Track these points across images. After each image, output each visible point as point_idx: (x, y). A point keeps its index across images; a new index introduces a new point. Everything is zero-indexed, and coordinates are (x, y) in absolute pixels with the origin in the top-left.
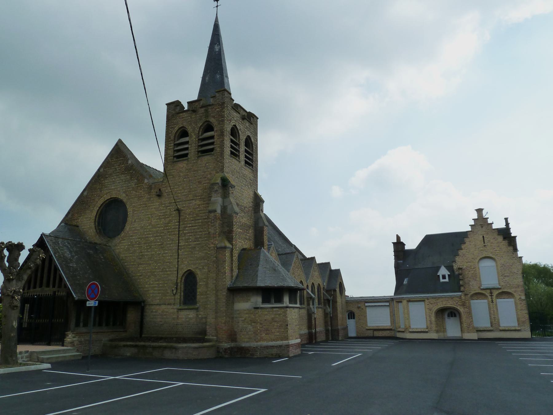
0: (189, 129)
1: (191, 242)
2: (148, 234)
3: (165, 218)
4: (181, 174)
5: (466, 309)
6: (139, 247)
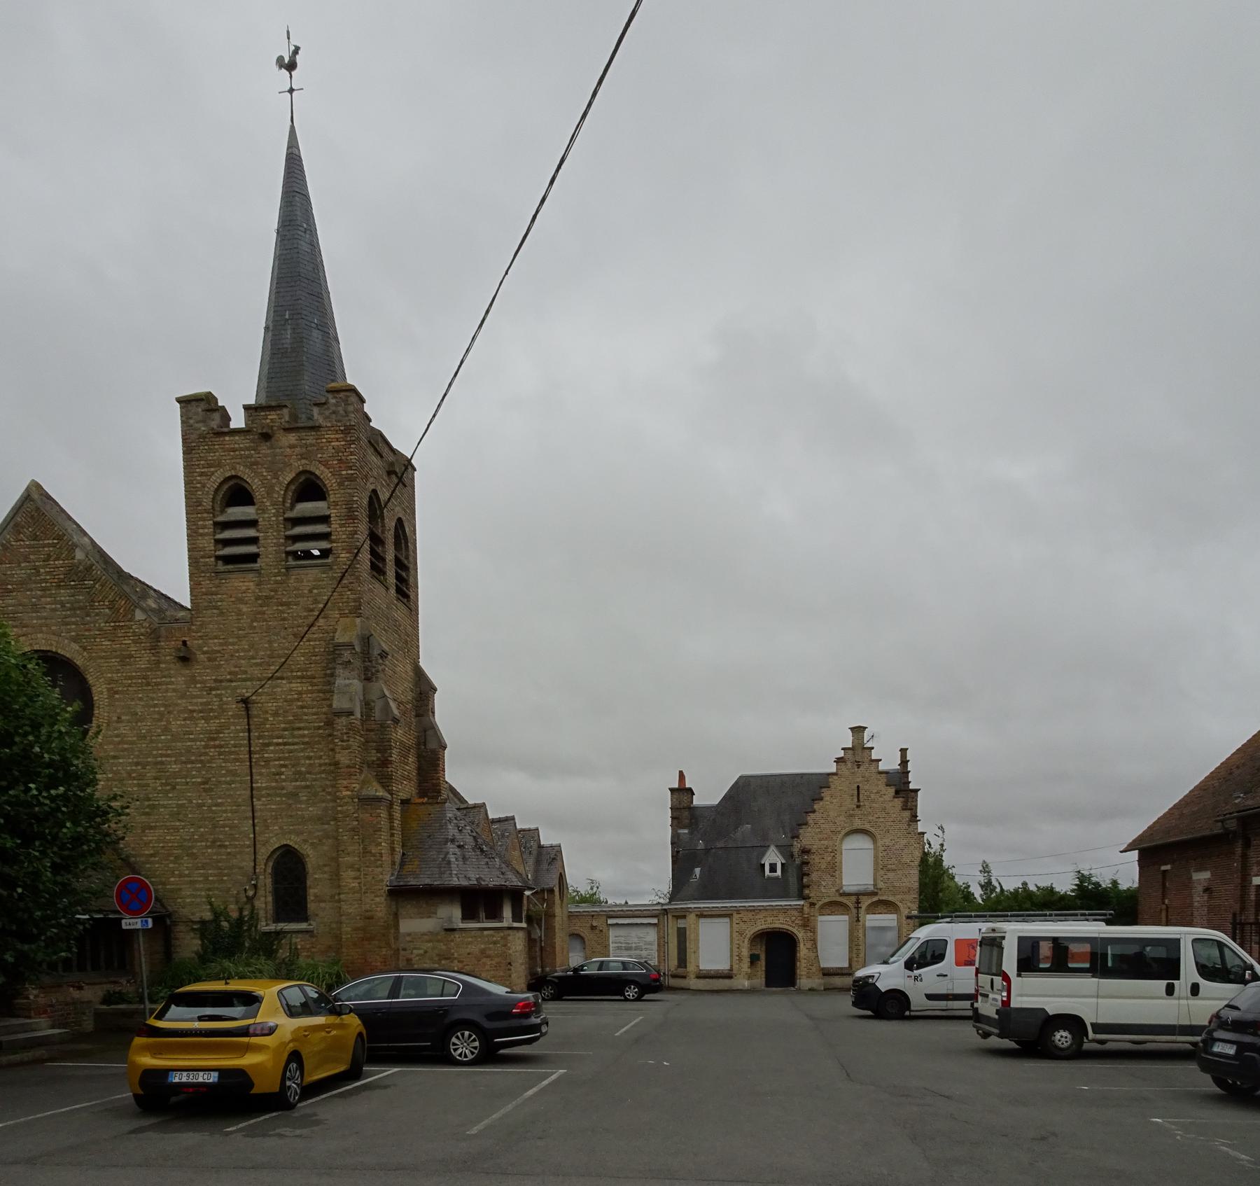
0: (256, 485)
1: (284, 781)
2: (162, 755)
3: (207, 719)
4: (245, 609)
5: (809, 934)
6: (139, 785)
